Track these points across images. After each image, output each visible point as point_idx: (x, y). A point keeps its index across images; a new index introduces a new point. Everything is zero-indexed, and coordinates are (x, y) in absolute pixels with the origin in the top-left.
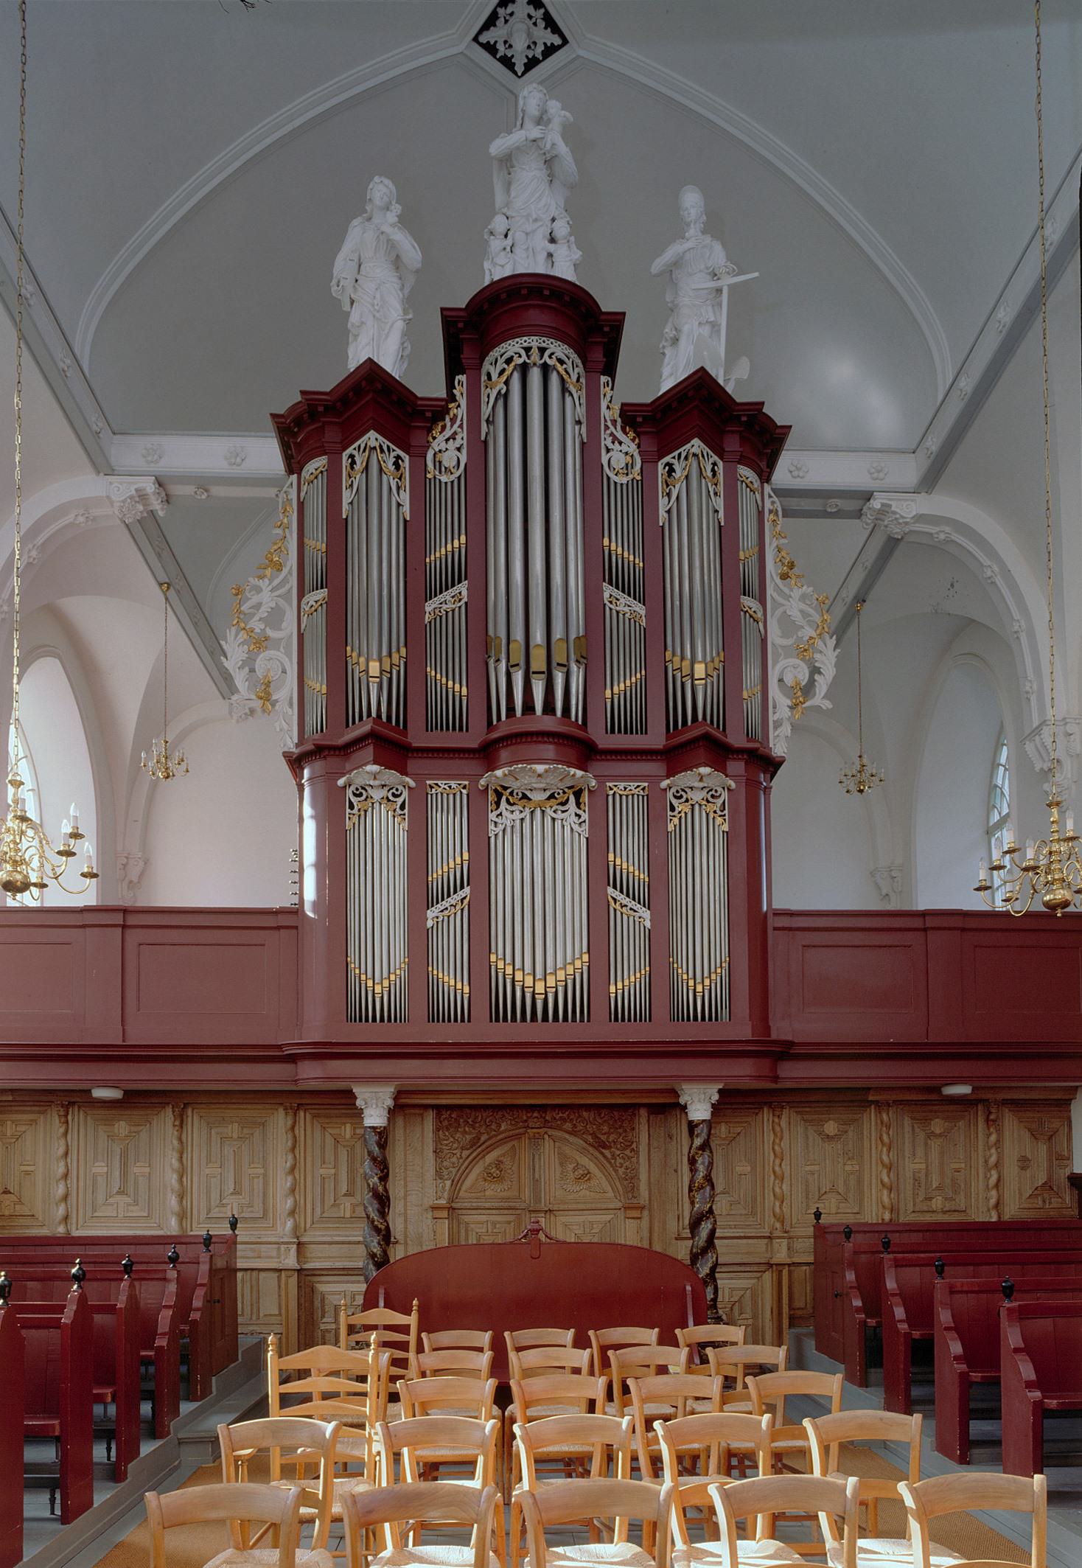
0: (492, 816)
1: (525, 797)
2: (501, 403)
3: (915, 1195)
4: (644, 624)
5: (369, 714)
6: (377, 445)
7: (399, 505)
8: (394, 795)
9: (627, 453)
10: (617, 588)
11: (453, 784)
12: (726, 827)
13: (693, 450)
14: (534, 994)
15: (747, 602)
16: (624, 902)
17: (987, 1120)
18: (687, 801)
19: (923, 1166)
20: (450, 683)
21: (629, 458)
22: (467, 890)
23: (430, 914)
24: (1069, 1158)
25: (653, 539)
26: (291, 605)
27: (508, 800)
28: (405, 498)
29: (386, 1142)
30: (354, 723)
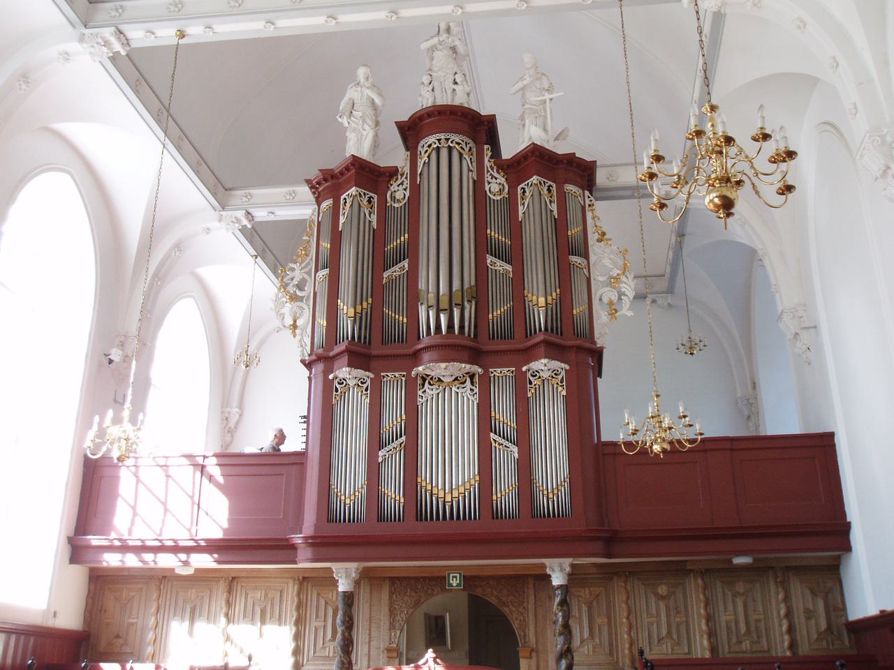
0: (420, 393)
1: (440, 380)
2: (426, 168)
3: (729, 640)
4: (511, 276)
5: (348, 338)
6: (358, 193)
7: (370, 222)
8: (362, 383)
9: (500, 184)
10: (496, 257)
11: (397, 374)
12: (565, 394)
13: (534, 182)
14: (444, 502)
15: (573, 259)
16: (501, 442)
17: (776, 582)
18: (540, 377)
19: (732, 617)
20: (397, 316)
21: (501, 187)
22: (404, 438)
23: (380, 453)
24: (844, 609)
25: (516, 229)
26: (310, 276)
27: (429, 383)
28: (374, 218)
29: (352, 603)
30: (340, 342)
